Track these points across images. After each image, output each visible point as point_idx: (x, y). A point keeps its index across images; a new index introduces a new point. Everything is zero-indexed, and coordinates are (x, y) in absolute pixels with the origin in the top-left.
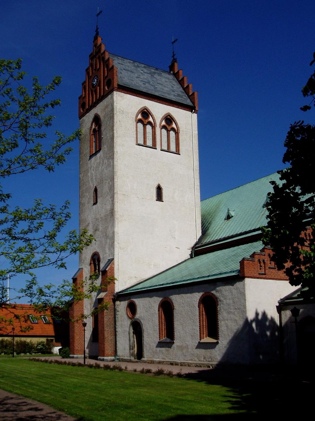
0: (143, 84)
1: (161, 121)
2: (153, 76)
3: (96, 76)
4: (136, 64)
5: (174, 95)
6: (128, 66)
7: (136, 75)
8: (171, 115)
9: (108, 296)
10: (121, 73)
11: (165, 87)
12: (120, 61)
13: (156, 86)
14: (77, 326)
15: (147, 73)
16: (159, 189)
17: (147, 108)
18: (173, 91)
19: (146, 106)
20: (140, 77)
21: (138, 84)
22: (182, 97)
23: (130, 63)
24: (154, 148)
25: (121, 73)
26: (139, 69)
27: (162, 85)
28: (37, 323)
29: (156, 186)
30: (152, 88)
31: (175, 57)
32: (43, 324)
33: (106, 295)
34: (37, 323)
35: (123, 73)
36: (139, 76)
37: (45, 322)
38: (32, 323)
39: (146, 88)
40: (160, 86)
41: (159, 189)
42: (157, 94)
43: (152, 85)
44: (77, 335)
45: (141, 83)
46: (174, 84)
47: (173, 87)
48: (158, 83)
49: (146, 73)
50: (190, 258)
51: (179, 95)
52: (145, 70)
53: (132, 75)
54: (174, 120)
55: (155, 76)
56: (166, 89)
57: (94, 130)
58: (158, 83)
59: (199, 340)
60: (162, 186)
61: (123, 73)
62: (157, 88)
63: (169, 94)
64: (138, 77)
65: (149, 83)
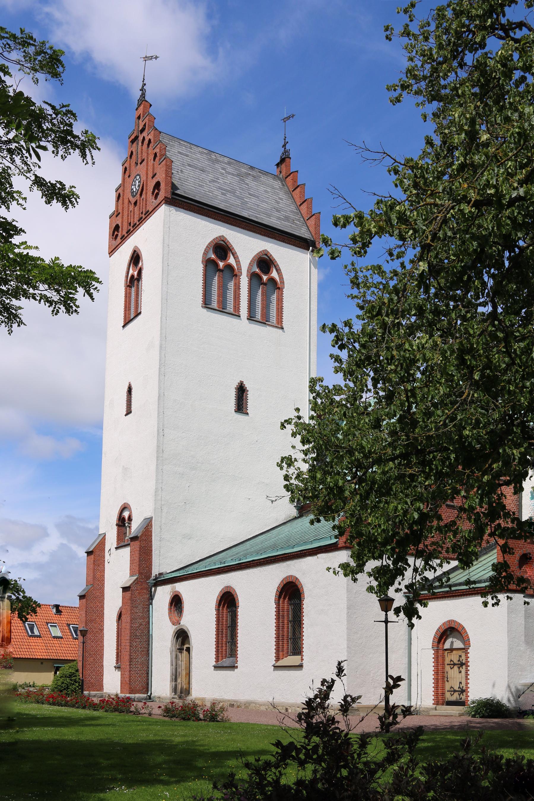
0: (223, 194)
1: (251, 264)
2: (243, 180)
3: (138, 175)
4: (214, 157)
5: (279, 218)
6: (198, 160)
7: (211, 177)
8: (269, 256)
9: (140, 583)
10: (181, 171)
11: (263, 201)
12: (183, 150)
13: (245, 199)
14: (90, 639)
15: (233, 174)
16: (241, 390)
17: (226, 239)
18: (278, 211)
19: (223, 236)
20: (219, 181)
21: (211, 194)
22: (293, 223)
23: (201, 153)
24: (236, 314)
25: (181, 171)
26: (217, 166)
27: (258, 197)
28: (39, 637)
29: (235, 384)
30: (238, 202)
31: (288, 147)
32: (72, 640)
33: (135, 580)
34: (39, 637)
35: (185, 171)
36: (216, 180)
37: (30, 634)
38: (30, 636)
39: (226, 202)
40: (254, 200)
41: (241, 390)
42: (246, 214)
43: (238, 197)
44: (90, 654)
45: (217, 193)
46: (281, 197)
47: (278, 203)
48: (250, 194)
49: (229, 173)
50: (296, 518)
51: (287, 219)
52: (230, 169)
53: (204, 176)
54: (275, 264)
55: (247, 181)
56: (265, 205)
57: (133, 276)
58: (250, 194)
59: (274, 662)
60: (247, 385)
61: (185, 171)
62: (246, 203)
63: (269, 216)
64: (214, 181)
65: (233, 192)
